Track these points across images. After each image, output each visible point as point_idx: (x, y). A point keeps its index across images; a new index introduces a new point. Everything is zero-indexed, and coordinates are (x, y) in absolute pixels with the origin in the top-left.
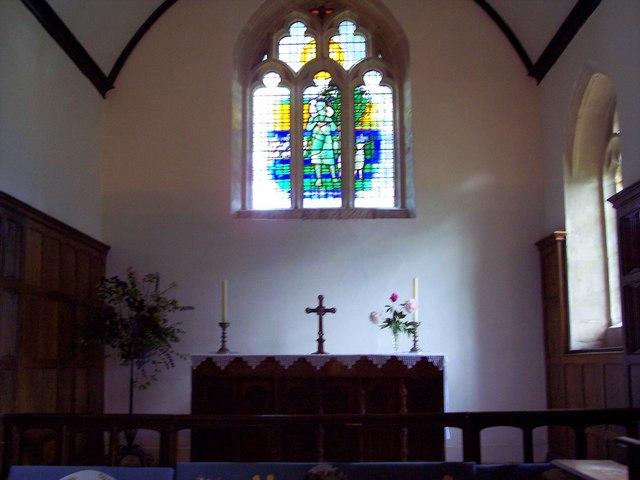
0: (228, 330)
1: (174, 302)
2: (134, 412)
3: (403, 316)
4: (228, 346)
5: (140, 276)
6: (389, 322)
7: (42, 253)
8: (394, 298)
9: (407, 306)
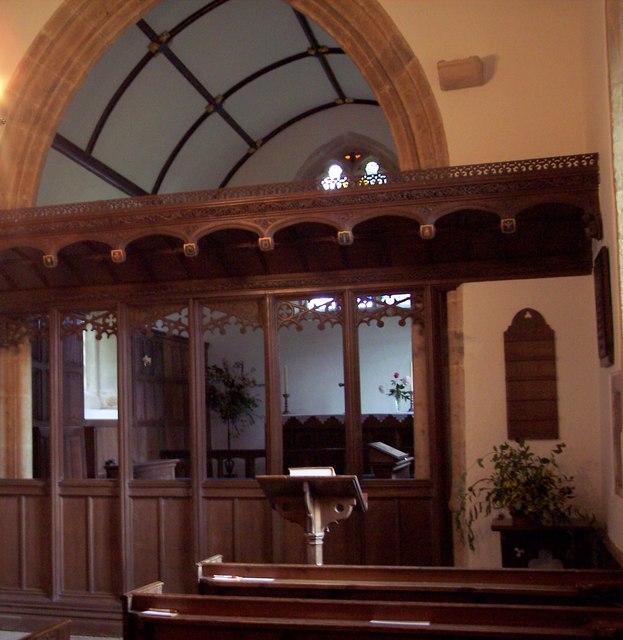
0: (288, 399)
1: (254, 382)
2: (231, 448)
3: (403, 387)
4: (289, 409)
5: (231, 363)
6: (392, 391)
7: (183, 279)
8: (396, 376)
9: (404, 381)
